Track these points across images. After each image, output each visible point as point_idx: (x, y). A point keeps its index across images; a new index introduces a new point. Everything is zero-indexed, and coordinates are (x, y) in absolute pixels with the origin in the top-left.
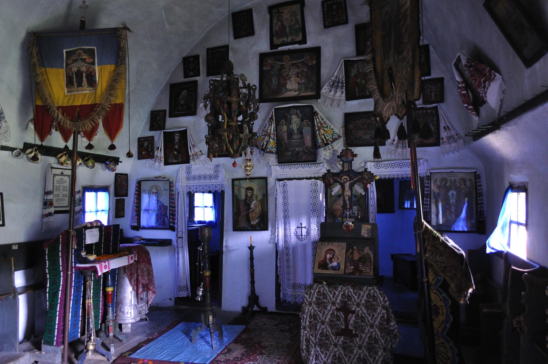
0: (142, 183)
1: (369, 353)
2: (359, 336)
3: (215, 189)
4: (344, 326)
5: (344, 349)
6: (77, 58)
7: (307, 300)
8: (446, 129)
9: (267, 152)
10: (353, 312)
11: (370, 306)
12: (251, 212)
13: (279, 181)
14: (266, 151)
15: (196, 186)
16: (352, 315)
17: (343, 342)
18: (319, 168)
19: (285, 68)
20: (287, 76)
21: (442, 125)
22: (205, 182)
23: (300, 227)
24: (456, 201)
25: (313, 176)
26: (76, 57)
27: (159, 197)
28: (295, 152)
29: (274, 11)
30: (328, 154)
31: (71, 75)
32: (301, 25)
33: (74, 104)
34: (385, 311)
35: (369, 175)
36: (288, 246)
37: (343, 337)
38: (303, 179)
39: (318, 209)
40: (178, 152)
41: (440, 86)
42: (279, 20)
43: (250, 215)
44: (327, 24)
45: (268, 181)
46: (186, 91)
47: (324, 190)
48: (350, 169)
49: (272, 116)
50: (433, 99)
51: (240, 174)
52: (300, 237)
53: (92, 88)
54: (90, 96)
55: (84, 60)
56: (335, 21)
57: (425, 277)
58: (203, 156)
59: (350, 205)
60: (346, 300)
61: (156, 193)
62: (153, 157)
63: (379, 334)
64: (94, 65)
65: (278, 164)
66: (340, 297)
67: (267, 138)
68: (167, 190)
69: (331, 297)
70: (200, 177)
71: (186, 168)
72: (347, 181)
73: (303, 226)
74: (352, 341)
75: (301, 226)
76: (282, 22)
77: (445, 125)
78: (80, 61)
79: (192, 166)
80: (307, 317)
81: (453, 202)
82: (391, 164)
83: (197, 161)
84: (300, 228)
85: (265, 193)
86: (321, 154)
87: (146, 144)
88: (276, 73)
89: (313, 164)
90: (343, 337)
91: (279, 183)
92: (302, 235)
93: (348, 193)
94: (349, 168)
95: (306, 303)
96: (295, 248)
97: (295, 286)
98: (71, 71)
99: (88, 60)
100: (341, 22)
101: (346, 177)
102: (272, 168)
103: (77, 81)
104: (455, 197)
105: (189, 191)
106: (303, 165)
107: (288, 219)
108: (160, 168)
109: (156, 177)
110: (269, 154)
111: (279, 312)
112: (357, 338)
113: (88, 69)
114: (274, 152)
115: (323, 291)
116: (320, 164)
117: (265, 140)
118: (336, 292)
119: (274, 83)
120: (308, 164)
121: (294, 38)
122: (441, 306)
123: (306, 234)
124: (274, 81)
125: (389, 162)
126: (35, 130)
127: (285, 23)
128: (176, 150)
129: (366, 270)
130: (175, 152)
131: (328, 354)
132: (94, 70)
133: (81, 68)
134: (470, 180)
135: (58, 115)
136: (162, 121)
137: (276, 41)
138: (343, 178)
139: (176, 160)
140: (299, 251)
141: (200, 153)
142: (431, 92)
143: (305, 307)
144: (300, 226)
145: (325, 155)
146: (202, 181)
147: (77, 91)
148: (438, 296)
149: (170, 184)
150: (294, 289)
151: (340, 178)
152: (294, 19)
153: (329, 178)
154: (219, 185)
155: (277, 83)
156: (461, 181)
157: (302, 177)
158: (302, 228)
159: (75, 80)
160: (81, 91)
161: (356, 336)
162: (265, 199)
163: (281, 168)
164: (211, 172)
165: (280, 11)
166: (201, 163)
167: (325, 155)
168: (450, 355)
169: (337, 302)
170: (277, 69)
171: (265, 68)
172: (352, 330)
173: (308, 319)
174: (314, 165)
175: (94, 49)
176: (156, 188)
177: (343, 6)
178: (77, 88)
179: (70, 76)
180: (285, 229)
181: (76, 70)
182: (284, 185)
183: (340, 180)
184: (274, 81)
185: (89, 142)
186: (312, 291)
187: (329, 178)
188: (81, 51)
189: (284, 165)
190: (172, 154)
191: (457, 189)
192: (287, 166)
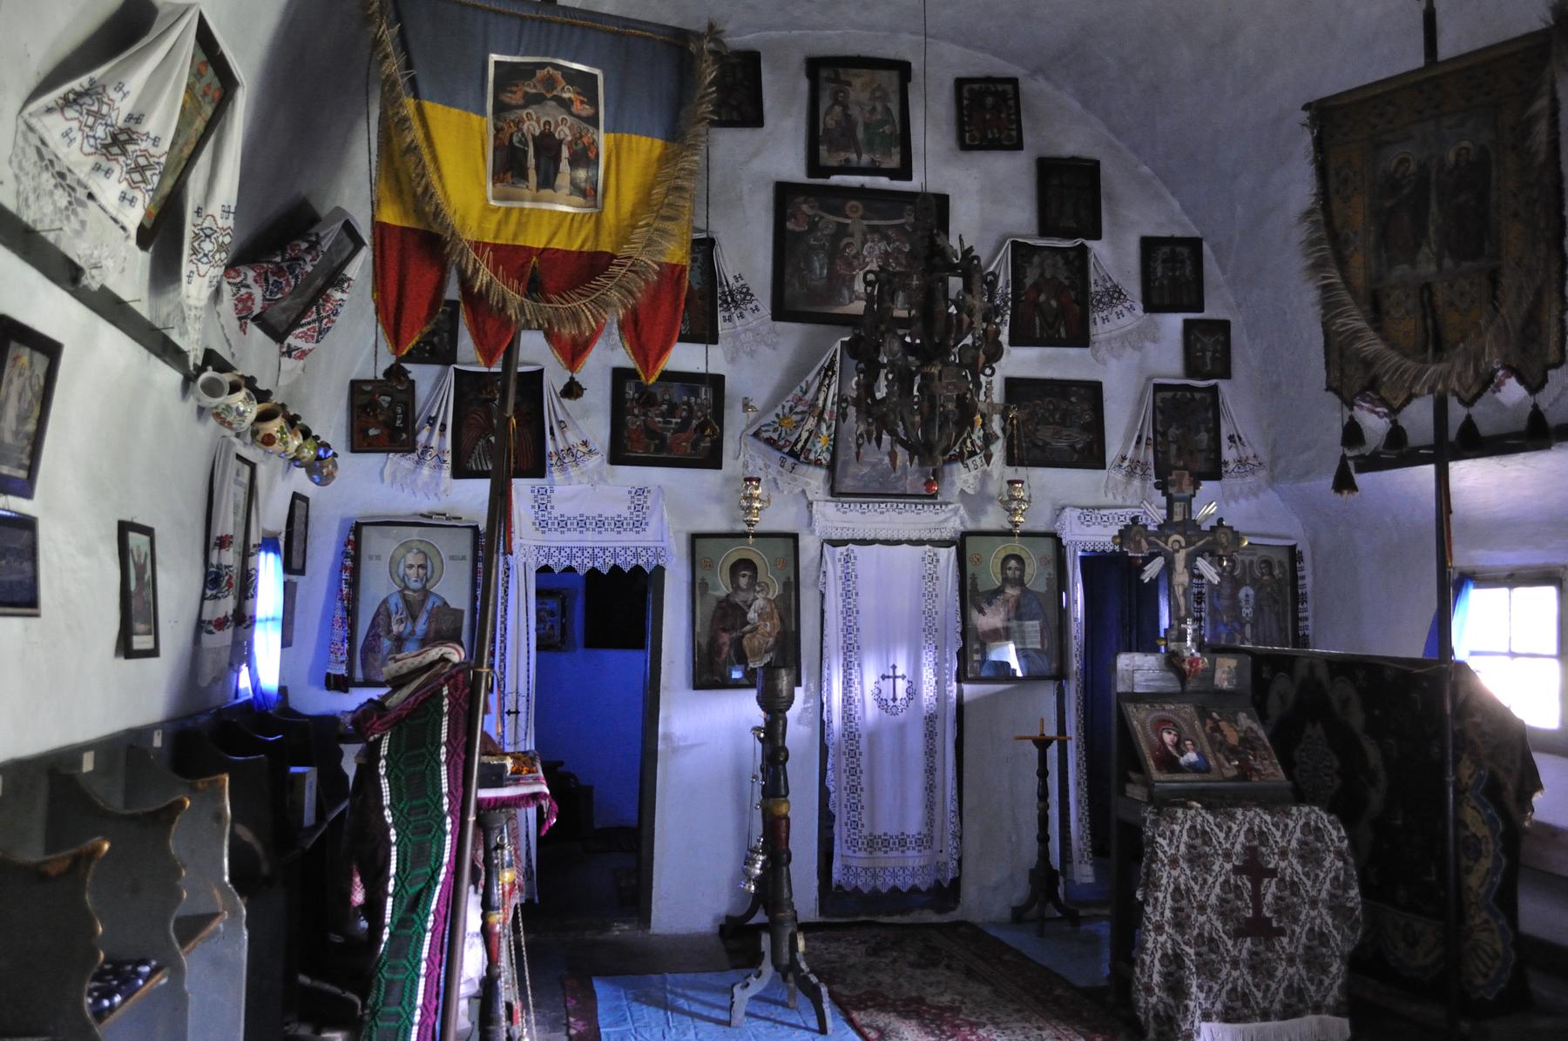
0: (365, 530)
1: (1254, 977)
2: (1288, 932)
3: (634, 562)
4: (1251, 911)
5: (1254, 969)
6: (543, 91)
7: (1165, 852)
8: (1234, 442)
9: (809, 463)
10: (1272, 873)
11: (1309, 856)
12: (750, 632)
13: (834, 546)
14: (806, 458)
16: (1270, 882)
17: (1252, 954)
18: (942, 516)
19: (852, 235)
20: (856, 256)
21: (1225, 431)
22: (599, 537)
23: (889, 677)
25: (925, 536)
26: (535, 87)
27: (432, 582)
28: (879, 467)
29: (824, 73)
30: (971, 481)
31: (520, 142)
32: (898, 126)
33: (519, 242)
34: (1340, 864)
35: (1230, 536)
36: (857, 730)
37: (1249, 940)
38: (898, 542)
39: (937, 626)
42: (836, 102)
43: (745, 642)
44: (967, 141)
45: (801, 544)
47: (955, 577)
49: (832, 362)
51: (716, 521)
52: (891, 703)
54: (576, 225)
55: (565, 104)
56: (990, 136)
57: (1451, 773)
58: (595, 457)
59: (1186, 608)
60: (1256, 843)
61: (419, 566)
62: (413, 450)
63: (1330, 921)
64: (597, 126)
65: (829, 498)
66: (1242, 838)
67: (811, 423)
68: (464, 558)
69: (1222, 840)
70: (582, 523)
71: (533, 491)
72: (1181, 547)
73: (899, 672)
74: (1270, 949)
75: (894, 672)
76: (845, 107)
77: (1233, 432)
78: (553, 103)
80: (1165, 897)
82: (1116, 517)
83: (573, 471)
84: (891, 680)
85: (792, 579)
86: (955, 478)
88: (824, 245)
89: (929, 504)
90: (1249, 940)
91: (834, 552)
92: (894, 699)
93: (1181, 577)
94: (1184, 515)
95: (1162, 861)
96: (874, 736)
97: (874, 843)
98: (520, 130)
99: (577, 108)
100: (1006, 143)
101: (1176, 537)
102: (814, 506)
103: (537, 168)
104: (1252, 600)
105: (615, 565)
106: (901, 506)
107: (856, 654)
108: (437, 484)
109: (422, 515)
110: (811, 469)
111: (829, 920)
112: (1282, 938)
113: (578, 138)
114: (824, 462)
115: (1203, 826)
116: (947, 504)
117: (807, 427)
118: (1233, 825)
119: (818, 272)
120: (916, 505)
121: (878, 157)
122: (1485, 836)
123: (905, 695)
124: (817, 265)
125: (1114, 511)
126: (377, 314)
127: (855, 112)
129: (1265, 769)
131: (1216, 988)
132: (594, 143)
133: (556, 128)
134: (1281, 564)
137: (827, 157)
138: (1171, 540)
140: (887, 743)
142: (1203, 350)
143: (1160, 870)
144: (891, 674)
145: (966, 481)
146: (589, 535)
147: (535, 200)
148: (1479, 812)
150: (871, 853)
151: (1163, 539)
152: (879, 107)
153: (1137, 538)
154: (647, 549)
155: (825, 271)
156: (1263, 565)
157: (896, 538)
158: (895, 677)
159: (531, 162)
160: (551, 201)
161: (1281, 932)
162: (793, 594)
163: (838, 510)
164: (623, 510)
165: (843, 77)
166: (585, 480)
167: (966, 481)
168: (1499, 946)
169: (1235, 850)
171: (790, 225)
172: (1270, 919)
173: (1169, 902)
174: (913, 506)
175: (595, 76)
176: (420, 551)
177: (1011, 103)
178: (538, 190)
180: (847, 683)
181: (537, 133)
182: (847, 559)
183: (1162, 544)
184: (819, 266)
185: (570, 374)
186: (1177, 828)
187: (1137, 538)
188: (558, 75)
189: (850, 503)
190: (482, 442)
191: (1256, 584)
192: (858, 505)
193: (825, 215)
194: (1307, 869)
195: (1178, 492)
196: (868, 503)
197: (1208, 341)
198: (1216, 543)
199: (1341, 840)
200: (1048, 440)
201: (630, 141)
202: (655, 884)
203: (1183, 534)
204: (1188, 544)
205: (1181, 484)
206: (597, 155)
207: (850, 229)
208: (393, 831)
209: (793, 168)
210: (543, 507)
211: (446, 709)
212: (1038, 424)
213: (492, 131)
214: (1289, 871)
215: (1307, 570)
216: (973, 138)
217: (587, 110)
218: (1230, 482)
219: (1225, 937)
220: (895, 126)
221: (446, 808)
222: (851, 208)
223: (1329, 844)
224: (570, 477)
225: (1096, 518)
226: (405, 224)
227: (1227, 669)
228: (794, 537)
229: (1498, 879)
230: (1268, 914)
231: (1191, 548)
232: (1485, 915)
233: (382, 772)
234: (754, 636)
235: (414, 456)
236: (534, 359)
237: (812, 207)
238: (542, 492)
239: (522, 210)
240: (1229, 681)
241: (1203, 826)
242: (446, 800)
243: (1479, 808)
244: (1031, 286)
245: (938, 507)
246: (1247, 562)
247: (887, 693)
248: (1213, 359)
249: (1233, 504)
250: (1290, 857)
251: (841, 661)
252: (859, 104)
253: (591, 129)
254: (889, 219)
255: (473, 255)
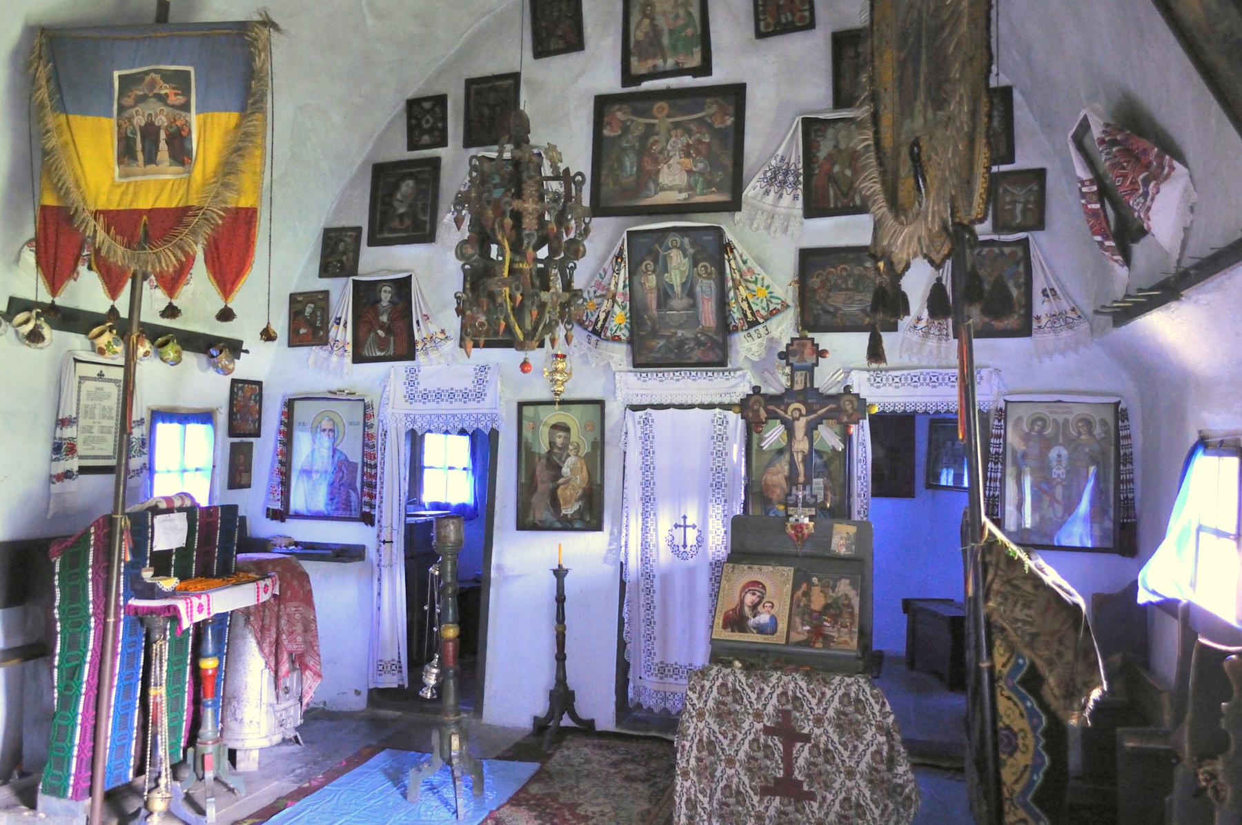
0: (297, 405)
3: (475, 426)
4: (782, 772)
7: (693, 705)
8: (1048, 296)
10: (806, 738)
11: (847, 726)
12: (563, 484)
15: (428, 417)
17: (781, 813)
18: (733, 382)
19: (657, 134)
21: (1038, 284)
22: (450, 406)
23: (680, 526)
24: (1068, 472)
25: (717, 400)
27: (338, 442)
30: (755, 348)
31: (132, 133)
33: (134, 206)
34: (883, 739)
35: (856, 404)
36: (652, 571)
37: (778, 799)
38: (691, 407)
40: (388, 330)
41: (1035, 188)
42: (645, 15)
43: (560, 492)
45: (607, 410)
46: (411, 183)
48: (808, 385)
49: (621, 250)
50: (1018, 221)
52: (682, 549)
53: (180, 169)
54: (176, 187)
56: (783, 20)
58: (449, 342)
60: (789, 707)
62: (326, 343)
63: (868, 794)
65: (632, 369)
66: (774, 700)
67: (606, 305)
69: (753, 700)
70: (439, 396)
72: (801, 415)
76: (652, 19)
77: (1045, 286)
78: (153, 100)
79: (421, 368)
80: (691, 747)
81: (1059, 475)
82: (909, 377)
83: (433, 355)
85: (599, 440)
87: (309, 310)
90: (778, 799)
92: (685, 546)
93: (801, 445)
94: (805, 384)
96: (666, 577)
98: (131, 124)
99: (173, 100)
100: (798, 24)
103: (143, 150)
104: (1064, 463)
106: (693, 374)
107: (652, 504)
109: (330, 392)
110: (610, 345)
111: (623, 731)
112: (812, 803)
114: (623, 338)
115: (734, 685)
116: (735, 370)
120: (641, 372)
121: (681, 59)
122: (1022, 730)
124: (628, 163)
125: (906, 372)
127: (661, 22)
128: (382, 327)
130: (380, 333)
134: (1104, 423)
135: (95, 231)
136: (351, 254)
138: (792, 407)
139: (382, 350)
140: (679, 583)
141: (442, 336)
142: (1014, 203)
143: (687, 721)
144: (682, 524)
145: (749, 350)
146: (444, 405)
147: (144, 174)
148: (1015, 704)
149: (365, 409)
151: (783, 407)
152: (682, 12)
153: (755, 407)
154: (485, 415)
155: (635, 169)
156: (1080, 424)
157: (689, 402)
158: (685, 527)
159: (139, 146)
161: (811, 796)
162: (599, 452)
164: (468, 383)
166: (442, 361)
167: (749, 350)
170: (636, 134)
175: (189, 72)
176: (331, 419)
179: (127, 138)
180: (645, 529)
181: (143, 123)
182: (646, 421)
184: (629, 164)
186: (707, 684)
188: (158, 77)
190: (372, 335)
193: (635, 118)
194: (844, 739)
195: (799, 360)
196: (664, 372)
197: (1019, 193)
198: (839, 410)
199: (885, 715)
200: (838, 305)
201: (212, 118)
202: (487, 683)
203: (804, 403)
204: (810, 412)
205: (803, 353)
206: (190, 132)
207: (657, 129)
208: (59, 624)
209: (610, 82)
210: (412, 383)
211: (92, 542)
212: (830, 290)
213: (116, 128)
214: (824, 738)
215: (1136, 424)
216: (767, 25)
217: (180, 100)
218: (1043, 338)
219: (751, 793)
220: (695, 27)
221: (91, 611)
222: (663, 109)
223: (871, 717)
224: (430, 360)
225: (887, 379)
226: (60, 205)
227: (845, 535)
228: (600, 403)
229: (1039, 779)
230: (800, 778)
231: (812, 416)
232: (1022, 814)
233: (57, 583)
234: (566, 489)
235: (328, 347)
236: (404, 267)
237: (624, 113)
238: (412, 371)
239: (136, 182)
240: (848, 548)
241: (734, 685)
242: (91, 606)
243: (1015, 699)
244: (825, 158)
245: (726, 373)
246: (1061, 421)
247: (679, 541)
248: (1025, 211)
249: (1047, 361)
250: (826, 724)
251: (640, 511)
252: (664, 13)
253: (183, 114)
254: (693, 113)
255: (93, 222)
